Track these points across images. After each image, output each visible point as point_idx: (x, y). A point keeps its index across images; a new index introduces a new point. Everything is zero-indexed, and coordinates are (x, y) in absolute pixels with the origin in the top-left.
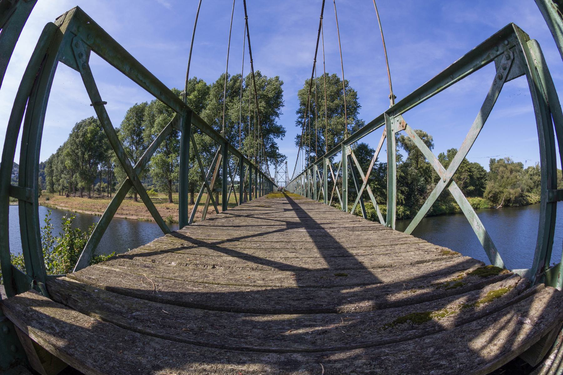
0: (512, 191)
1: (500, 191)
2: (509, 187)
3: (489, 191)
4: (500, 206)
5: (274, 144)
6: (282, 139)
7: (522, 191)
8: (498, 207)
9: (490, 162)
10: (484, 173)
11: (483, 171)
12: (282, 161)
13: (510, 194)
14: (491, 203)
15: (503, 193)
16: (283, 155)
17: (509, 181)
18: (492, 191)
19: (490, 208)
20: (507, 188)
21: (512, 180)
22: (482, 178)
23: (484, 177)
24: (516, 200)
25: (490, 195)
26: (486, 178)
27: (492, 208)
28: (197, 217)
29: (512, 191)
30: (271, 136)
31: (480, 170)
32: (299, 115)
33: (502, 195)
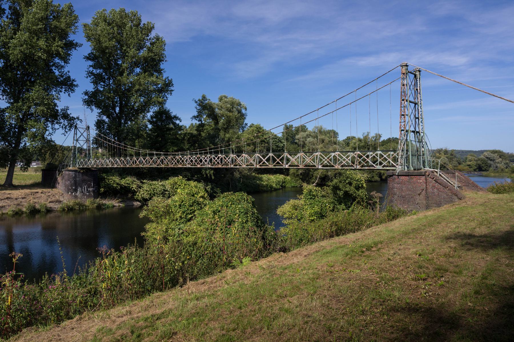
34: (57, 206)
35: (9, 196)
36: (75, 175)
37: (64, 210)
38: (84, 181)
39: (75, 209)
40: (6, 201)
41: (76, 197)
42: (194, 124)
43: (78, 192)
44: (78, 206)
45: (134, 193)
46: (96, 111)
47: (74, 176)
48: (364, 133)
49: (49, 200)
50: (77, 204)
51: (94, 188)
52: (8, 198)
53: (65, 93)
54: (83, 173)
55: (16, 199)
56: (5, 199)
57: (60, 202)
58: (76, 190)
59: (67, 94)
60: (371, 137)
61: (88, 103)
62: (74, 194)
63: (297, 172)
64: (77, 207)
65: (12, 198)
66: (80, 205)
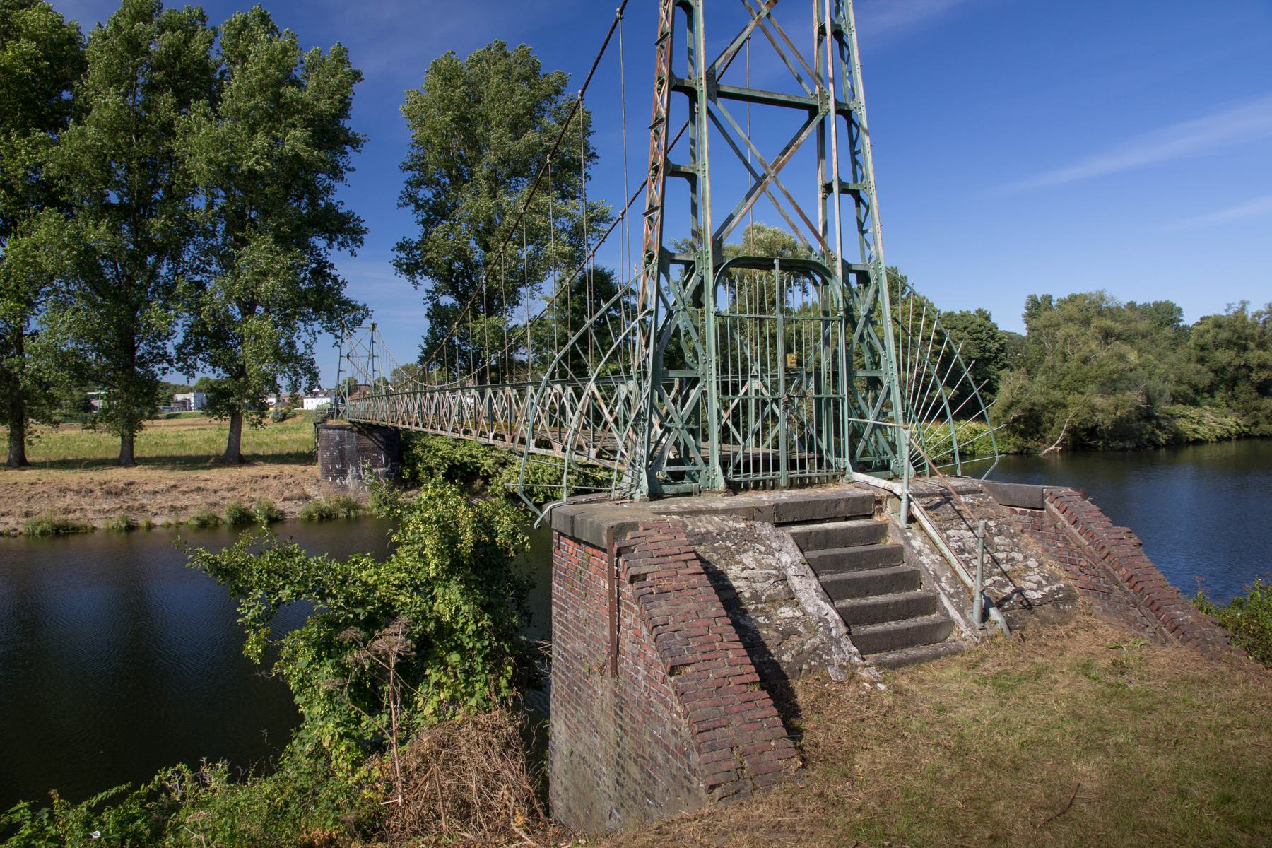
0: (1099, 401)
1: (1052, 403)
2: (1093, 387)
3: (1007, 402)
4: (1053, 447)
5: (325, 267)
6: (352, 253)
7: (1150, 399)
8: (1045, 451)
9: (1027, 308)
10: (997, 345)
11: (993, 334)
12: (357, 323)
13: (1093, 410)
14: (1017, 440)
15: (1065, 406)
16: (360, 304)
17: (1091, 369)
18: (1019, 402)
19: (1016, 453)
20: (1082, 393)
21: (1100, 366)
22: (988, 361)
23: (996, 357)
24: (1121, 430)
25: (1013, 414)
26: (1007, 361)
27: (1022, 453)
28: (66, 509)
29: (1099, 401)
30: (320, 243)
31: (983, 336)
32: (409, 174)
33: (1060, 413)
34: (295, 510)
35: (202, 485)
36: (341, 437)
37: (311, 518)
38: (361, 451)
39: (337, 517)
40: (194, 495)
41: (344, 488)
42: (810, 304)
43: (349, 476)
44: (344, 510)
45: (487, 478)
46: (428, 283)
47: (338, 439)
48: (1229, 305)
49: (287, 494)
50: (343, 505)
51: (386, 466)
52: (199, 489)
53: (339, 249)
54: (359, 432)
55: (215, 492)
56: (192, 491)
57: (307, 498)
58: (343, 473)
59: (346, 251)
60: (1250, 316)
61: (410, 269)
62: (338, 481)
63: (1004, 416)
64: (341, 513)
65: (207, 490)
66: (351, 506)
